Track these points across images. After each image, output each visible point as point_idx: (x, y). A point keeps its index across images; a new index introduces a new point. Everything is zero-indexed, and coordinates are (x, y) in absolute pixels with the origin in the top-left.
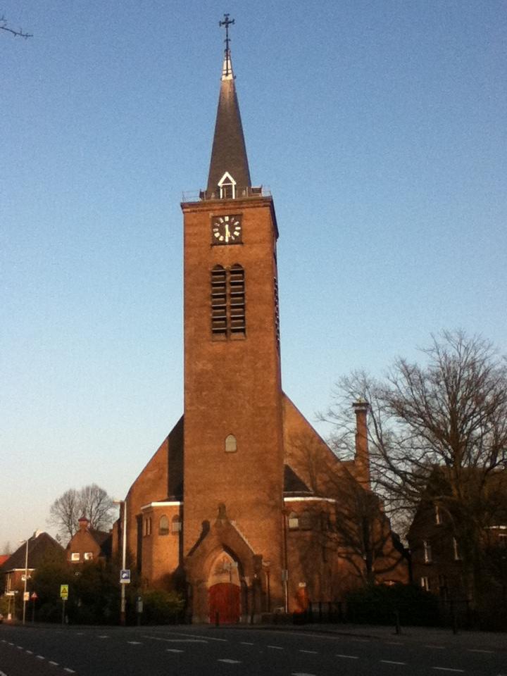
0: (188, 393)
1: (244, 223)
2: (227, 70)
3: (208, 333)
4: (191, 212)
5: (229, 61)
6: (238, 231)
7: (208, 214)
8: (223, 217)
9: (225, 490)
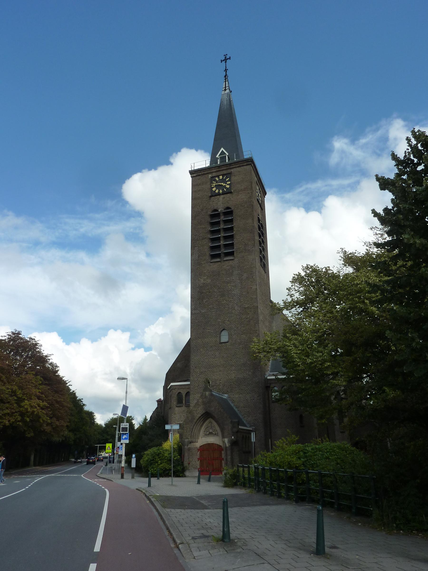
0: (193, 301)
1: (233, 178)
2: (225, 87)
3: (208, 257)
4: (196, 176)
5: (227, 82)
6: (372, 402)
7: (208, 176)
8: (218, 176)
9: (220, 371)
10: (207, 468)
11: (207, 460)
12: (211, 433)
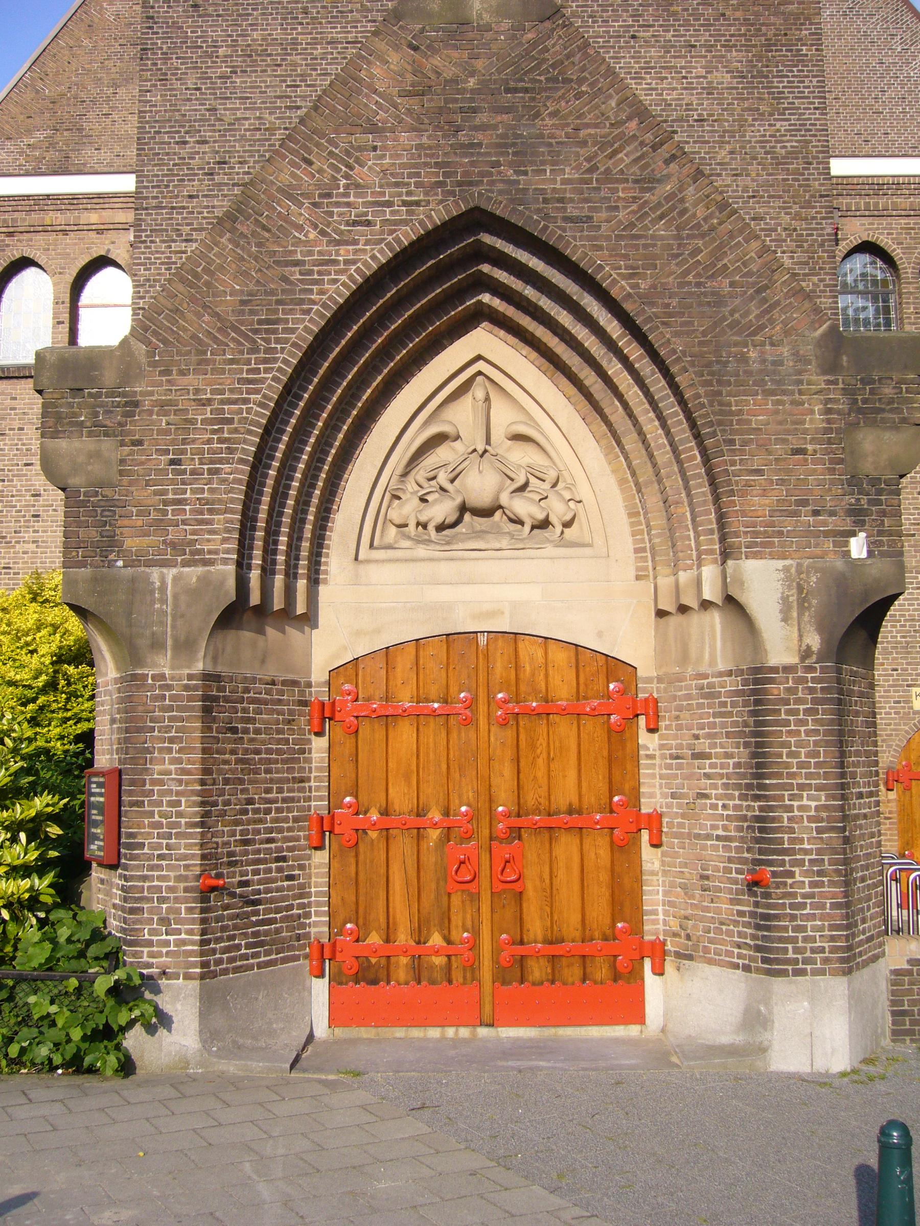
10: (436, 940)
11: (434, 835)
12: (486, 513)
